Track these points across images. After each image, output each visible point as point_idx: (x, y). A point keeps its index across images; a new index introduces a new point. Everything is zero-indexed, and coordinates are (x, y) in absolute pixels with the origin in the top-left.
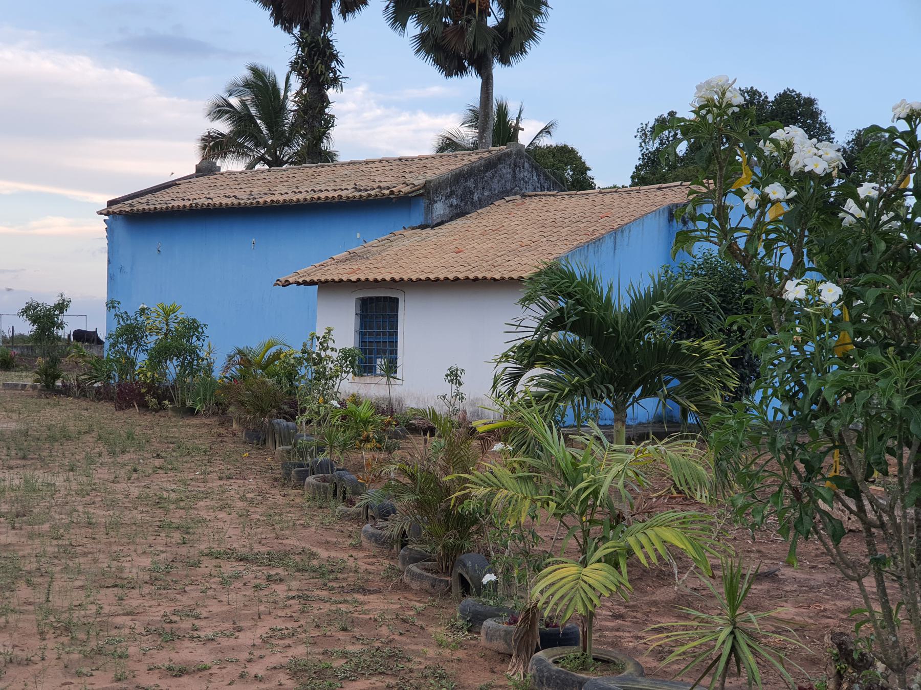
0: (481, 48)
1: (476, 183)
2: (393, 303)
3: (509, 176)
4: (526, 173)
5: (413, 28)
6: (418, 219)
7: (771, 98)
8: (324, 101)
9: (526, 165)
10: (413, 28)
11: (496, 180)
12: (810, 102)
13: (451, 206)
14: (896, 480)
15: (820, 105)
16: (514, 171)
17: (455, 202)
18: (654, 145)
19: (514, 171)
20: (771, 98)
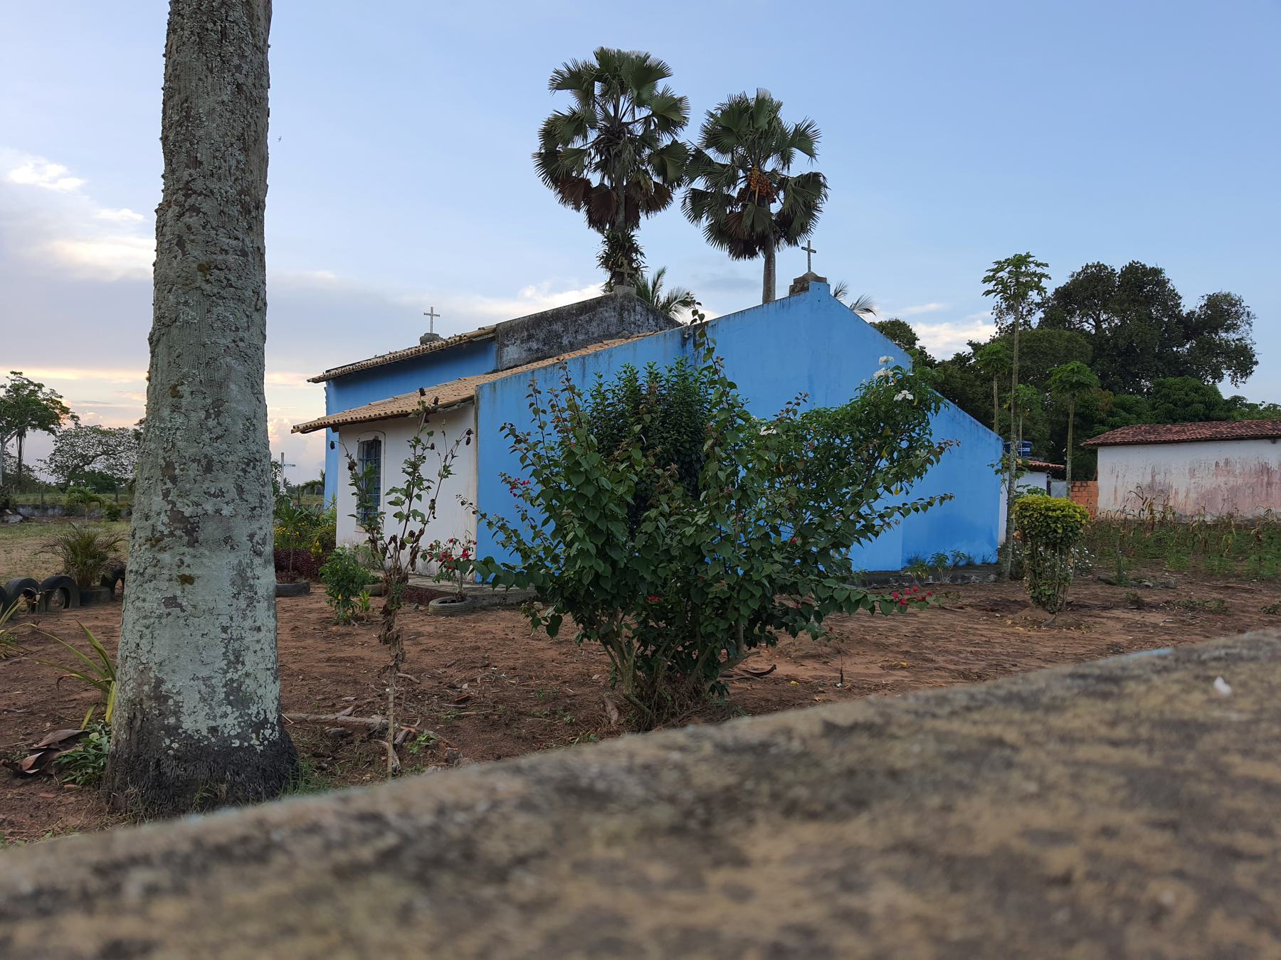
0: (759, 229)
1: (565, 325)
2: (1095, 452)
3: (614, 320)
4: (638, 317)
5: (705, 222)
6: (491, 365)
7: (1118, 271)
8: (922, 352)
9: (638, 308)
10: (705, 222)
11: (594, 324)
12: (1156, 272)
13: (530, 349)
14: (636, 479)
15: (1167, 275)
16: (621, 315)
17: (535, 346)
18: (1010, 320)
19: (621, 315)
20: (1118, 271)
